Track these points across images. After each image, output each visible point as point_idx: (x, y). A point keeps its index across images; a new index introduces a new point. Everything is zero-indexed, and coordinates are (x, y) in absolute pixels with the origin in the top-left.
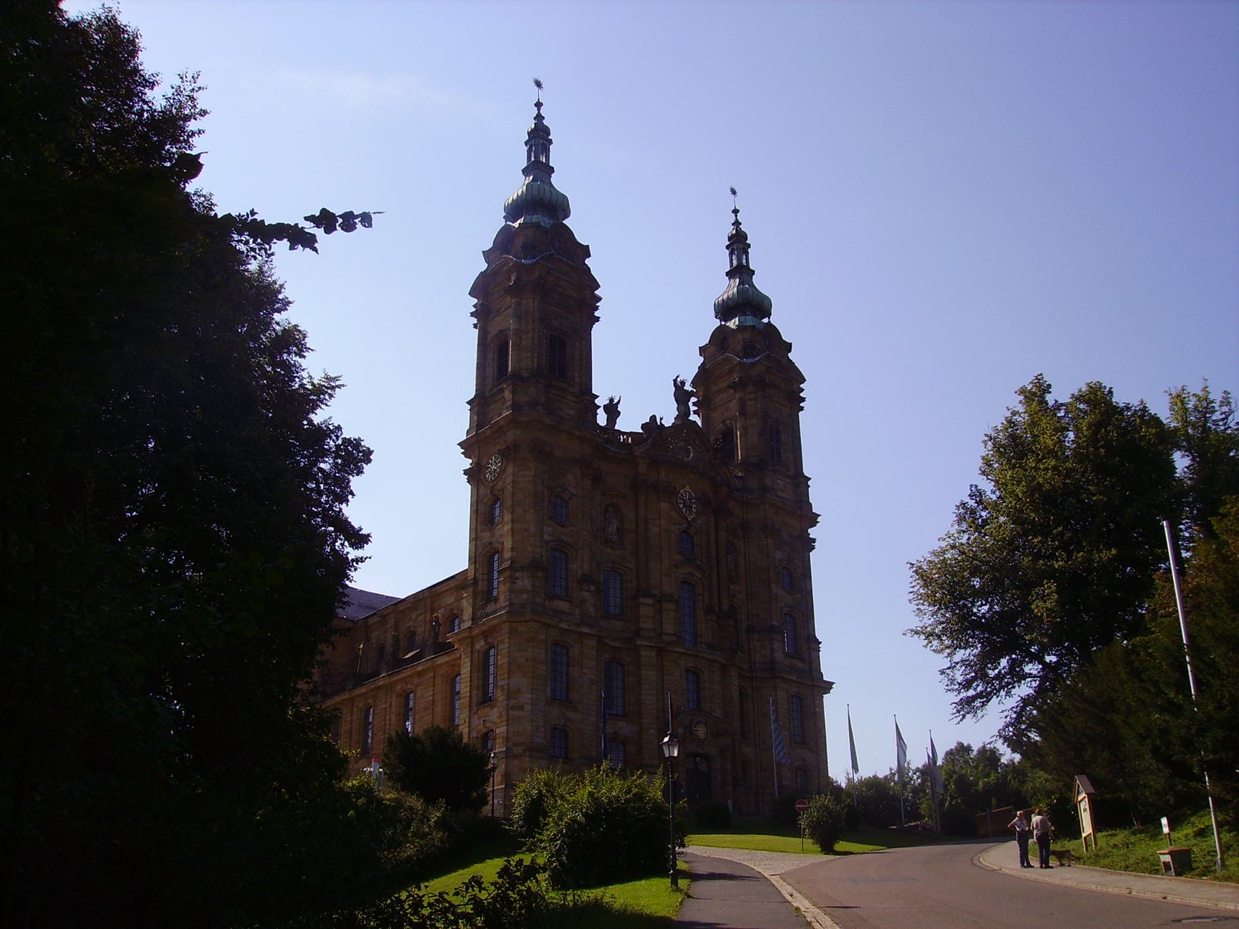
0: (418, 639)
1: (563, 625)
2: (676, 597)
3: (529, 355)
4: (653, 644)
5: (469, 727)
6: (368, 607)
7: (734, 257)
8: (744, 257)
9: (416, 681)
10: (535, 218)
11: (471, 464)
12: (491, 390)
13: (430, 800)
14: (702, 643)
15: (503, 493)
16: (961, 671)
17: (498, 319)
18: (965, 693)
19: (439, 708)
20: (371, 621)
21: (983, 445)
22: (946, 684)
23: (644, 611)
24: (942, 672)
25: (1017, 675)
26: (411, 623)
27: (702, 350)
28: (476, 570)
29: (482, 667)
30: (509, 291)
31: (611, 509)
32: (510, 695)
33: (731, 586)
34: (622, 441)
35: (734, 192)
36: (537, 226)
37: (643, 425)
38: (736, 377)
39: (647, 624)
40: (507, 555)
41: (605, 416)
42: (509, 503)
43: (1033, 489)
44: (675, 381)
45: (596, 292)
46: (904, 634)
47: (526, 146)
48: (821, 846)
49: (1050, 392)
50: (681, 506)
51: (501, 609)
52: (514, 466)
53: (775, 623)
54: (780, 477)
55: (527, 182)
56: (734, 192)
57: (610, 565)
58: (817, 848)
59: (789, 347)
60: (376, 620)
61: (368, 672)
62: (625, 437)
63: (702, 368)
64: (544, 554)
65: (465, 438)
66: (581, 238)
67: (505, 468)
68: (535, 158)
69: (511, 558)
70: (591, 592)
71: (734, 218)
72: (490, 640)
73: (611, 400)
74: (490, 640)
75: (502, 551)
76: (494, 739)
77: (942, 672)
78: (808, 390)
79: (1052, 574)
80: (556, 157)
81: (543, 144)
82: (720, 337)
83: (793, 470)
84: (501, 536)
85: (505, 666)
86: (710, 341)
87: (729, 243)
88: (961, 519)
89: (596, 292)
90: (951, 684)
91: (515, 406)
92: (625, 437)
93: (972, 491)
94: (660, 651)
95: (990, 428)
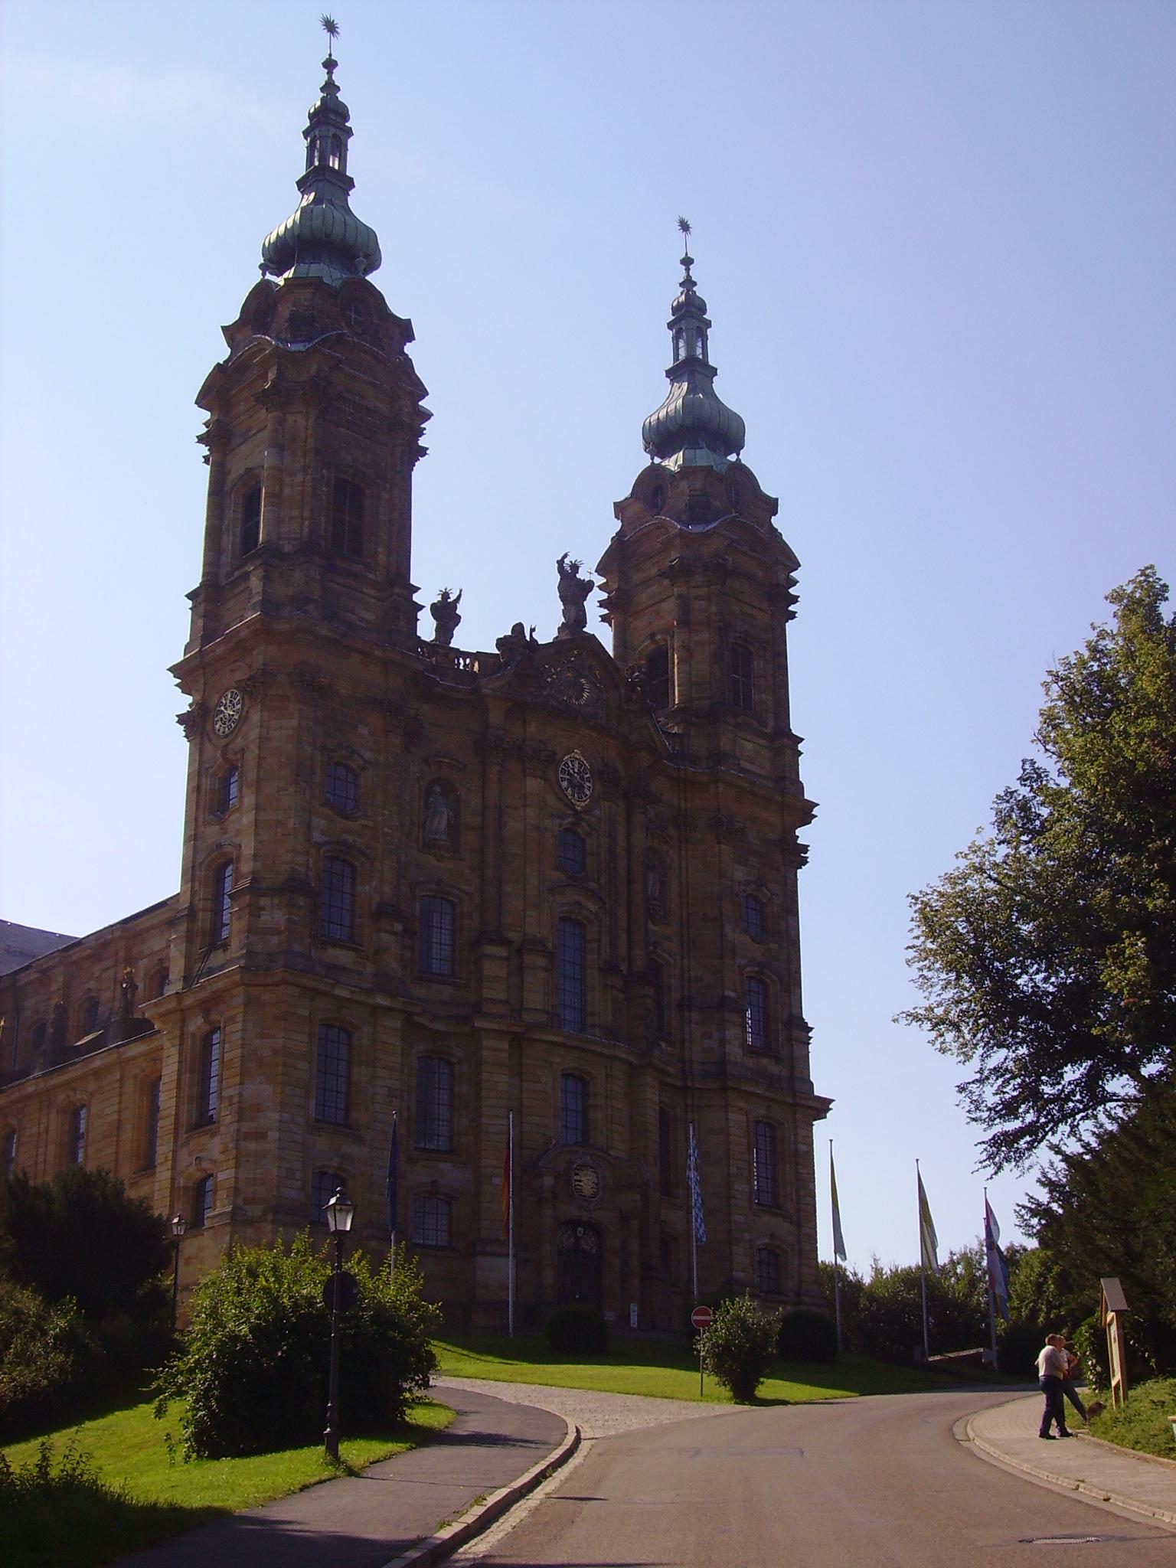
0: (103, 1010)
1: (342, 992)
2: (550, 945)
3: (295, 512)
4: (505, 1028)
5: (173, 1168)
6: (22, 954)
7: (681, 344)
8: (700, 344)
9: (92, 1086)
10: (315, 270)
11: (190, 705)
12: (229, 574)
13: (52, 1297)
14: (593, 1026)
15: (242, 758)
16: (996, 1087)
17: (245, 449)
18: (1000, 1126)
19: (128, 1134)
20: (24, 979)
21: (1043, 690)
22: (967, 1109)
23: (491, 969)
24: (962, 1089)
25: (1093, 1093)
26: (92, 985)
27: (620, 509)
28: (193, 893)
29: (198, 1065)
30: (264, 399)
31: (438, 789)
32: (243, 1113)
33: (651, 926)
34: (461, 667)
35: (685, 227)
36: (317, 284)
37: (499, 640)
38: (674, 557)
39: (495, 992)
40: (246, 867)
41: (434, 623)
42: (251, 776)
43: (1113, 773)
44: (561, 563)
45: (420, 403)
46: (894, 1021)
47: (306, 138)
48: (732, 1390)
49: (1167, 599)
50: (565, 784)
51: (232, 962)
52: (261, 710)
54: (749, 737)
55: (304, 203)
56: (685, 227)
57: (434, 886)
58: (726, 1392)
59: (772, 506)
60: (32, 977)
61: (17, 1068)
62: (468, 661)
63: (618, 540)
64: (311, 866)
65: (182, 658)
66: (398, 306)
67: (247, 712)
68: (319, 161)
69: (253, 873)
70: (395, 934)
71: (684, 274)
72: (214, 1017)
73: (445, 595)
74: (214, 1017)
75: (238, 859)
76: (215, 1191)
77: (962, 1089)
78: (806, 584)
79: (1141, 922)
81: (335, 136)
82: (651, 485)
83: (771, 723)
84: (238, 832)
85: (237, 1063)
86: (632, 493)
87: (673, 318)
88: (1002, 821)
89: (420, 403)
90: (977, 1108)
91: (268, 605)
92: (468, 661)
93: (1024, 770)
94: (518, 1041)
95: (1057, 662)
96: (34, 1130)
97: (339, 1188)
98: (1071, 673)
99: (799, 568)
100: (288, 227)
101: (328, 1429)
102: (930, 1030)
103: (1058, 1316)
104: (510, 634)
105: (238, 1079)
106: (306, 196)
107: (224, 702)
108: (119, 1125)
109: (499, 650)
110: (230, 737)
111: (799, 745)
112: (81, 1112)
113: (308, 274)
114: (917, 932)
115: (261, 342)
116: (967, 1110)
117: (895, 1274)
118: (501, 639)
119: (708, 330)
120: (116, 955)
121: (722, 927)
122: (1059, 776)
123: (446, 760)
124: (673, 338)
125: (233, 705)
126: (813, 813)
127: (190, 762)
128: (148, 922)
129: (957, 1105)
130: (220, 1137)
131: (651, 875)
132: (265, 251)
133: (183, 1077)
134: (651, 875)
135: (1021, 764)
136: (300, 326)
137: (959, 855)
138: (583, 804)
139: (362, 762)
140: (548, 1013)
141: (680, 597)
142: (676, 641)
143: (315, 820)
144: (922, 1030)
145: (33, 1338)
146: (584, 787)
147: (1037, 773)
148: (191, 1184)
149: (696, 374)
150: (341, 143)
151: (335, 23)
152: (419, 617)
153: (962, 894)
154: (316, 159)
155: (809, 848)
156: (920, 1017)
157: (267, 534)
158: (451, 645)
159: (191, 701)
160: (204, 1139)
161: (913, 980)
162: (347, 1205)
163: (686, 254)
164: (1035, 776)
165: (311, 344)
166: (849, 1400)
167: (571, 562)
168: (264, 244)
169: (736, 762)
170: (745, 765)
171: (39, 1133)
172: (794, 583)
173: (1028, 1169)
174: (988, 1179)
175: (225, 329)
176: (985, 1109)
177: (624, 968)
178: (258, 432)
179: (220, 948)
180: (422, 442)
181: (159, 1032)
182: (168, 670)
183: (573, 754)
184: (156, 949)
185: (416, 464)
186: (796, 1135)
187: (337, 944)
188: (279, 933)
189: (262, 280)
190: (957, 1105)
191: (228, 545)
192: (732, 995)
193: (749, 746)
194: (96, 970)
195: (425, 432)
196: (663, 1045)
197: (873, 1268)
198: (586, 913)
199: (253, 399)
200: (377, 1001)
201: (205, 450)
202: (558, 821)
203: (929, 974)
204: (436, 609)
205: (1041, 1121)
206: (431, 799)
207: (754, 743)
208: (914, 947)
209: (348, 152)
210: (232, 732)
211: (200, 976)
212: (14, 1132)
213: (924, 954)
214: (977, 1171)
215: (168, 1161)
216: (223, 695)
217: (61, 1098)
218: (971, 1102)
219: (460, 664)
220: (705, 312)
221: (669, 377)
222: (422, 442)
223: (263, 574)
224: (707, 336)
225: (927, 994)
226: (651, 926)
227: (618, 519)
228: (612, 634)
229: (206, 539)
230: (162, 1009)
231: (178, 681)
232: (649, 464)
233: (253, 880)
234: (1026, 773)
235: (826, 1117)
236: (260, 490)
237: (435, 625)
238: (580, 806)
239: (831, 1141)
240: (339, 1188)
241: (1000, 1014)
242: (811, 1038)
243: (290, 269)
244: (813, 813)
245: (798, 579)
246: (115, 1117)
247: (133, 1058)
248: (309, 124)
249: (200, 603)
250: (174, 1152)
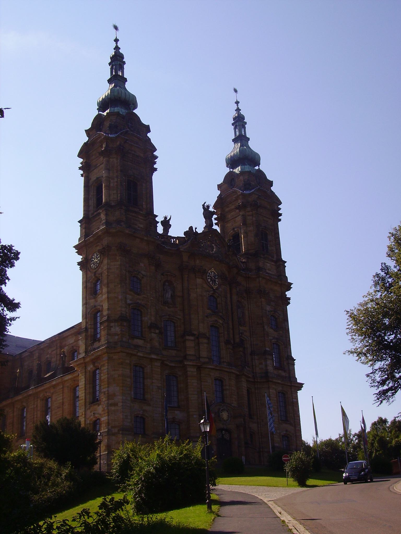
0: (53, 365)
2: (208, 335)
3: (115, 192)
4: (195, 364)
5: (85, 417)
7: (237, 130)
8: (243, 130)
10: (116, 109)
12: (92, 214)
13: (62, 462)
14: (224, 362)
16: (379, 374)
18: (382, 388)
19: (66, 407)
21: (388, 239)
22: (370, 382)
24: (368, 376)
26: (48, 356)
27: (219, 187)
28: (86, 323)
30: (102, 154)
31: (167, 284)
32: (110, 396)
33: (240, 327)
34: (172, 242)
35: (236, 91)
36: (118, 114)
38: (240, 202)
39: (191, 352)
40: (105, 313)
42: (105, 281)
44: (203, 205)
45: (154, 153)
46: (344, 354)
48: (298, 482)
50: (209, 280)
51: (102, 345)
52: (107, 259)
53: (268, 349)
55: (111, 87)
56: (236, 91)
57: (168, 317)
58: (296, 483)
59: (271, 183)
60: (27, 354)
62: (174, 240)
63: (220, 197)
66: (145, 121)
67: (102, 260)
71: (236, 107)
72: (96, 364)
73: (166, 218)
74: (96, 364)
75: (102, 311)
76: (100, 424)
77: (368, 376)
78: (283, 209)
80: (250, 132)
82: (229, 178)
83: (275, 257)
84: (101, 301)
87: (234, 122)
88: (376, 284)
89: (154, 153)
90: (374, 382)
91: (108, 223)
92: (174, 240)
93: (382, 266)
94: (199, 368)
95: (392, 229)
96: (33, 406)
97: (204, 417)
98: (397, 233)
99: (282, 204)
100: (106, 95)
101: (208, 501)
102: (356, 356)
103: (379, 454)
104: (188, 230)
105: (107, 386)
106: (111, 85)
107: (94, 257)
108: (63, 403)
109: (185, 236)
110: (97, 269)
111: (285, 264)
112: (49, 400)
113: (114, 111)
114: (349, 323)
115: (99, 134)
116: (370, 383)
117: (321, 442)
118: (185, 232)
119: (246, 125)
120: (57, 346)
122: (394, 268)
123: (169, 274)
124: (234, 128)
125: (97, 258)
126: (291, 287)
127: (82, 278)
128: (65, 335)
129: (367, 381)
130: (101, 405)
132: (98, 104)
133: (87, 386)
135: (381, 264)
136: (113, 128)
137: (364, 296)
138: (216, 287)
139: (142, 276)
141: (243, 215)
142: (242, 231)
143: (128, 296)
144: (354, 356)
145: (58, 477)
146: (216, 281)
147: (386, 267)
148: (92, 422)
149: (243, 140)
150: (122, 67)
151: (117, 26)
152: (157, 226)
153: (367, 309)
154: (114, 72)
155: (291, 299)
156: (353, 352)
157: (106, 199)
158: (168, 235)
159: (82, 257)
160: (97, 406)
161: (349, 339)
162: (207, 422)
163: (237, 100)
164: (386, 268)
165: (117, 135)
166: (336, 484)
167: (207, 205)
168: (98, 102)
169: (265, 270)
170: (268, 271)
171: (34, 408)
172: (280, 209)
173: (392, 402)
174: (377, 406)
175: (86, 131)
176: (376, 382)
177: (232, 342)
179: (97, 341)
180: (155, 166)
181: (76, 371)
182: (73, 247)
183: (211, 270)
184: (71, 343)
185: (153, 174)
187: (137, 338)
188: (118, 335)
189: (98, 113)
190: (367, 381)
191: (92, 204)
193: (268, 265)
194: (50, 351)
195: (156, 163)
197: (313, 441)
199: (98, 154)
200: (152, 357)
201: (82, 172)
202: (208, 293)
203: (354, 337)
204: (162, 222)
205: (395, 386)
206: (165, 287)
207: (270, 264)
208: (348, 328)
209: (124, 70)
210: (97, 267)
211: (91, 351)
212: (25, 407)
213: (354, 331)
214: (375, 403)
215: (83, 415)
216: (93, 255)
217: (41, 395)
218: (371, 380)
219: (172, 241)
220: (244, 119)
221: (233, 142)
222: (155, 166)
223: (105, 213)
224: (245, 127)
225: (354, 344)
226: (240, 327)
227: (219, 190)
229: (84, 202)
230: (78, 363)
231: (77, 251)
232: (229, 171)
233: (108, 317)
234: (383, 267)
235: (301, 390)
236: (102, 185)
237: (163, 228)
238: (215, 287)
239: (312, 397)
240: (204, 417)
241: (379, 350)
242: (295, 363)
243: (108, 109)
244: (291, 287)
245: (281, 208)
246: (61, 401)
247: (67, 380)
248: (110, 61)
249: (83, 224)
250: (85, 411)
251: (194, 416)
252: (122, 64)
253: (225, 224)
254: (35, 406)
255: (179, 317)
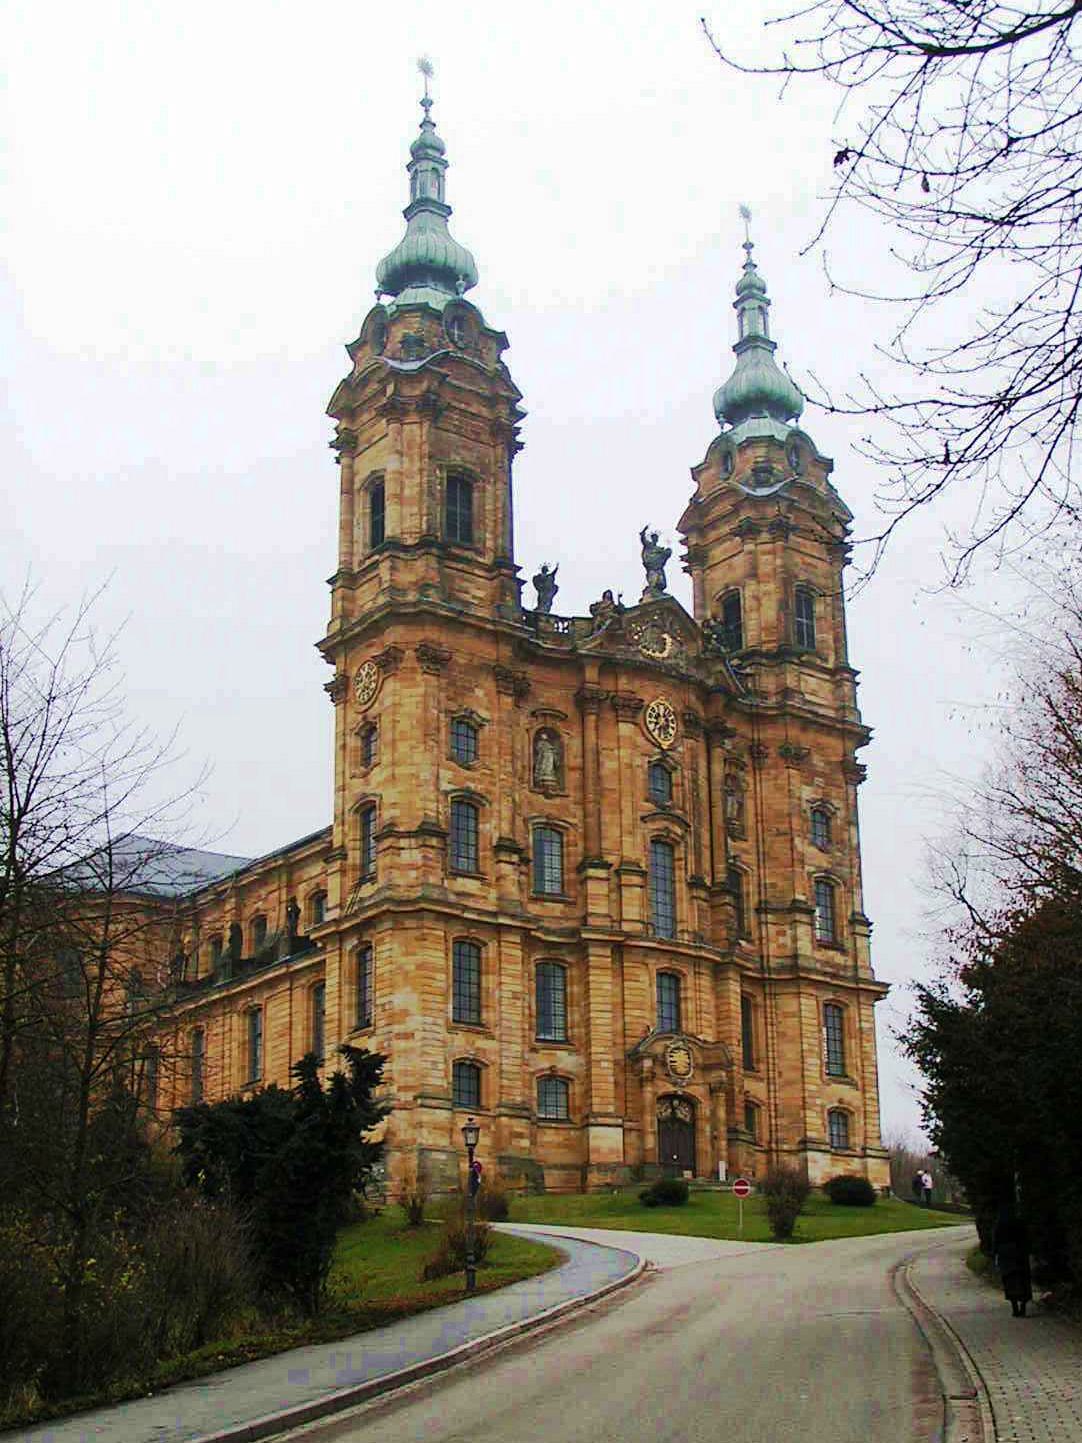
3: (415, 510)
7: (745, 322)
12: (361, 562)
19: (299, 1033)
31: (544, 736)
44: (643, 534)
66: (494, 321)
70: (513, 863)
71: (424, 115)
110: (369, 704)
121: (792, 840)
131: (730, 798)
134: (730, 798)
140: (643, 922)
170: (808, 697)
177: (708, 881)
178: (381, 439)
186: (860, 1015)
188: (417, 868)
192: (803, 898)
196: (743, 943)
198: (672, 835)
204: (537, 581)
228: (691, 585)
251: (604, 1064)
252: (440, 167)
253: (708, 571)
254: (226, 1029)
255: (571, 820)
